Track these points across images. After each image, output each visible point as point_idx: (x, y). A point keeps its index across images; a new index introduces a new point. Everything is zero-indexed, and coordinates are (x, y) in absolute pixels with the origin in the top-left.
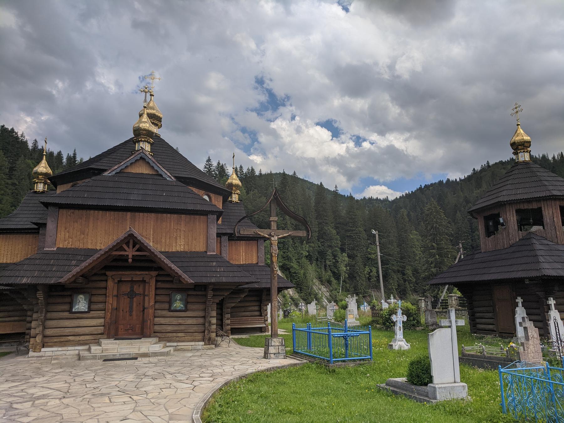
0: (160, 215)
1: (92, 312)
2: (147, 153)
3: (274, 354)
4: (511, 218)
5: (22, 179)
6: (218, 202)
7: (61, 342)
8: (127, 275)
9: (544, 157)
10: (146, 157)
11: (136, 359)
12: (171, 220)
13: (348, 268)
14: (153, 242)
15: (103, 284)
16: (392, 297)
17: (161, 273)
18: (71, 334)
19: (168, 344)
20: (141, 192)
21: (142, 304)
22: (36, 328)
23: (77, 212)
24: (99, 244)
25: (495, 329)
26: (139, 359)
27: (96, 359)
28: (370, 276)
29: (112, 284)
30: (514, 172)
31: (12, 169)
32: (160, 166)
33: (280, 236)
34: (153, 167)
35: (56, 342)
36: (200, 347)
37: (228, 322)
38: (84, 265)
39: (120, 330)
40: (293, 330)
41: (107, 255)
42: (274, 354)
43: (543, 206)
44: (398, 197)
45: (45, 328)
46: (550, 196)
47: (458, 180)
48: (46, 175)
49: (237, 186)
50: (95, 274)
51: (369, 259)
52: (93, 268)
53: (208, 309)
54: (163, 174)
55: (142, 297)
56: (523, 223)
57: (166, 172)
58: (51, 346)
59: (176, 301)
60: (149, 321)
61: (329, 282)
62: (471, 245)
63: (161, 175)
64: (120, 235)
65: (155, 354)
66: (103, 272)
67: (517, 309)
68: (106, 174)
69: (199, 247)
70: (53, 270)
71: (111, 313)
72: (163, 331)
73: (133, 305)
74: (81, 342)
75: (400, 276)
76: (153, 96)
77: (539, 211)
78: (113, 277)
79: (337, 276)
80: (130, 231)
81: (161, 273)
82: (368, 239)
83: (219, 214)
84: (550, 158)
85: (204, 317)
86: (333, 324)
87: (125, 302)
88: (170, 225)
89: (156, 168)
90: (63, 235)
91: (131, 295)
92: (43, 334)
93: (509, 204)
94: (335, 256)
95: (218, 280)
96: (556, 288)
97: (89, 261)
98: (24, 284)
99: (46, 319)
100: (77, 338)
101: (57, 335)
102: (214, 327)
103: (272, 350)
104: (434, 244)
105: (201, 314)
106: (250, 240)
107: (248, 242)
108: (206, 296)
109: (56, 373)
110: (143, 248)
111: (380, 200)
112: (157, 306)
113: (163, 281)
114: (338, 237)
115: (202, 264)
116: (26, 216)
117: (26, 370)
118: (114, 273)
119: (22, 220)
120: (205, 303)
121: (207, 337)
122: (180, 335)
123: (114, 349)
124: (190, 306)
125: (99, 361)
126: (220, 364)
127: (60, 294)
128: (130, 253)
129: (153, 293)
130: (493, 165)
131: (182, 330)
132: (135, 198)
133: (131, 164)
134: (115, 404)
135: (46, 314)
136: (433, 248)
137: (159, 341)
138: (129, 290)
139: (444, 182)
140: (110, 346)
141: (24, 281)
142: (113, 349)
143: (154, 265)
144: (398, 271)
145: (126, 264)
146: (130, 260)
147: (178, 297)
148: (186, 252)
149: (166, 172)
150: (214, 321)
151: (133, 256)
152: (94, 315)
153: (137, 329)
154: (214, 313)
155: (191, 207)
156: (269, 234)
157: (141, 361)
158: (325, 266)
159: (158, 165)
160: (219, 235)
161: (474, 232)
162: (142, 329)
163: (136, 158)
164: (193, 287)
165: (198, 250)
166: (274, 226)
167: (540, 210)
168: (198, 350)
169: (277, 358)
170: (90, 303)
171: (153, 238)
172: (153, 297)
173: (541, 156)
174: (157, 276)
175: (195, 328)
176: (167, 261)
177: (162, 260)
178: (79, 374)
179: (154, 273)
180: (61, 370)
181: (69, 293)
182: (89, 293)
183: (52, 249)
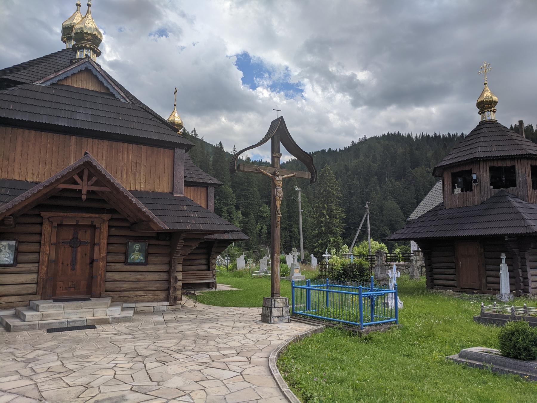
0: (115, 144)
3: (278, 317)
4: (482, 175)
8: (71, 218)
9: (409, 136)
10: (92, 69)
11: (93, 327)
13: (242, 224)
15: (37, 228)
16: (327, 252)
17: (116, 216)
19: (125, 305)
24: (30, 175)
25: (456, 285)
28: (261, 232)
30: (483, 130)
34: (101, 83)
36: (164, 308)
42: (278, 317)
43: (516, 164)
44: (285, 162)
46: (527, 154)
47: (338, 150)
50: (24, 215)
51: (261, 217)
52: (25, 207)
55: (89, 247)
56: (495, 183)
57: (119, 91)
59: (134, 252)
62: (348, 208)
63: (113, 95)
65: (118, 320)
66: (36, 212)
67: (501, 265)
69: (163, 186)
71: (47, 267)
72: (117, 289)
74: (4, 305)
75: (287, 233)
76: (80, 6)
77: (512, 170)
81: (116, 216)
82: (261, 199)
84: (414, 137)
91: (75, 243)
93: (489, 160)
96: (532, 246)
97: (25, 194)
104: (325, 205)
105: (165, 268)
110: (102, 179)
112: (110, 258)
114: (234, 195)
115: (171, 207)
118: (52, 214)
121: (172, 295)
122: (138, 293)
123: (59, 314)
124: (151, 259)
125: (40, 332)
128: (85, 186)
129: (104, 241)
130: (369, 139)
132: (82, 118)
133: (73, 75)
136: (324, 208)
138: (71, 237)
139: (326, 151)
140: (51, 311)
142: (57, 314)
144: (286, 229)
146: (84, 197)
147: (137, 247)
148: (148, 193)
149: (119, 91)
152: (24, 269)
155: (155, 137)
161: (352, 197)
163: (80, 68)
165: (161, 190)
167: (514, 167)
168: (162, 313)
169: (281, 322)
170: (17, 252)
172: (105, 246)
173: (407, 134)
175: (158, 285)
176: (134, 200)
177: (130, 198)
179: (107, 217)
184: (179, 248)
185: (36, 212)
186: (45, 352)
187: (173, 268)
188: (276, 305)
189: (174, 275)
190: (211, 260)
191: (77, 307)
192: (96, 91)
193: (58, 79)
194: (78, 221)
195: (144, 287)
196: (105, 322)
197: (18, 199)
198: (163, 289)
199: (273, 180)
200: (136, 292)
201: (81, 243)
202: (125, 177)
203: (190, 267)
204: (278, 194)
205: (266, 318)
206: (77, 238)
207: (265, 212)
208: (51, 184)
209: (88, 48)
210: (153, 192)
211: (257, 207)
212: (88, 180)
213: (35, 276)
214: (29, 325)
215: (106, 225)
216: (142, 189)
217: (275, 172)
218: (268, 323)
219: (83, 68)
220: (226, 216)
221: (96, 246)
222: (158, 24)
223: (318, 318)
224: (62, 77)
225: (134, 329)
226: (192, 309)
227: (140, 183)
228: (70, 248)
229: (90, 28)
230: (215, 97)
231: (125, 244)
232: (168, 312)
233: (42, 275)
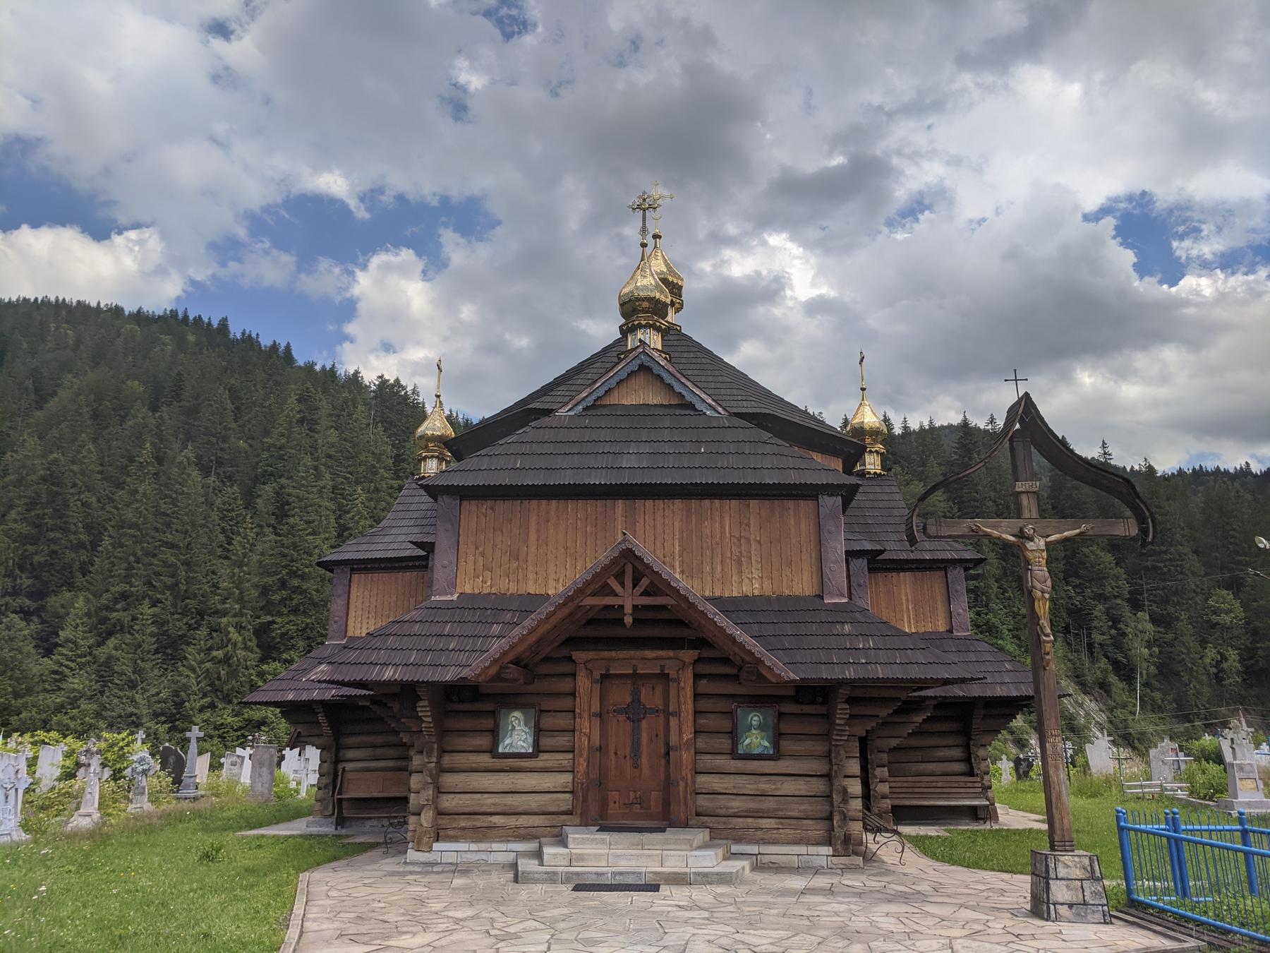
0: (694, 503)
1: (543, 756)
2: (656, 354)
3: (1071, 906)
7: (476, 828)
8: (623, 661)
11: (655, 888)
12: (722, 519)
13: (1156, 649)
14: (682, 572)
15: (565, 685)
17: (707, 653)
18: (498, 809)
19: (735, 848)
20: (647, 448)
22: (419, 790)
23: (500, 505)
24: (552, 583)
26: (664, 890)
27: (555, 882)
28: (1222, 670)
31: (398, 459)
32: (688, 384)
34: (670, 387)
35: (464, 828)
36: (823, 862)
37: (884, 788)
38: (517, 632)
39: (611, 805)
40: (1121, 829)
41: (572, 606)
42: (1071, 906)
45: (439, 791)
50: (546, 659)
51: (1214, 626)
53: (838, 754)
54: (695, 401)
55: (661, 719)
57: (703, 396)
58: (454, 839)
60: (682, 784)
61: (1104, 686)
63: (691, 406)
64: (603, 555)
65: (706, 879)
66: (565, 652)
69: (801, 584)
70: (451, 647)
73: (639, 739)
74: (522, 832)
76: (660, 237)
78: (589, 665)
79: (1126, 672)
80: (624, 541)
81: (707, 653)
82: (1206, 574)
85: (828, 776)
86: (1185, 804)
87: (620, 730)
88: (722, 527)
89: (678, 388)
90: (471, 566)
91: (635, 712)
94: (1115, 621)
98: (388, 683)
99: (443, 771)
100: (512, 821)
101: (467, 810)
102: (857, 804)
103: (1059, 891)
106: (925, 569)
107: (919, 574)
108: (828, 717)
109: (457, 921)
110: (658, 586)
111: (1226, 472)
112: (702, 743)
113: (712, 677)
114: (1121, 571)
115: (814, 628)
116: (405, 530)
117: (391, 904)
118: (590, 655)
119: (395, 541)
120: (827, 736)
121: (839, 833)
124: (787, 745)
125: (563, 888)
126: (901, 928)
127: (466, 707)
128: (628, 599)
129: (688, 706)
131: (769, 810)
132: (633, 464)
135: (439, 757)
138: (628, 700)
141: (388, 674)
142: (595, 855)
143: (686, 633)
145: (617, 632)
146: (628, 620)
147: (755, 719)
148: (768, 599)
149: (703, 396)
150: (855, 787)
151: (635, 607)
152: (550, 764)
153: (652, 803)
154: (854, 767)
156: (1016, 531)
157: (672, 896)
158: (1090, 646)
159: (683, 380)
160: (851, 555)
162: (667, 803)
163: (629, 369)
164: (791, 692)
166: (1029, 507)
168: (817, 871)
169: (1080, 919)
170: (538, 732)
172: (691, 717)
174: (695, 662)
175: (805, 807)
176: (721, 620)
178: (512, 930)
179: (689, 655)
180: (469, 912)
181: (488, 706)
182: (533, 706)
183: (448, 598)
184: (842, 722)
185: (565, 652)
186: (543, 926)
187: (835, 768)
188: (1062, 872)
189: (836, 783)
190: (973, 749)
191: (634, 845)
192: (661, 405)
193: (593, 397)
196: (679, 879)
199: (1022, 548)
200: (760, 821)
201: (646, 712)
202: (719, 569)
203: (922, 767)
204: (1037, 584)
205: (1040, 907)
206: (639, 701)
207: (1228, 612)
208: (569, 599)
209: (645, 326)
210: (780, 597)
211: (1198, 599)
212: (634, 586)
213: (568, 777)
214: (547, 873)
215: (689, 673)
216: (757, 593)
217: (1021, 530)
218: (1042, 918)
219: (634, 366)
220: (1105, 629)
221: (671, 718)
222: (901, 193)
223: (1195, 920)
224: (601, 393)
225: (727, 900)
226: (892, 868)
229: (645, 288)
230: (1075, 320)
231: (730, 713)
232: (830, 870)
233: (580, 776)
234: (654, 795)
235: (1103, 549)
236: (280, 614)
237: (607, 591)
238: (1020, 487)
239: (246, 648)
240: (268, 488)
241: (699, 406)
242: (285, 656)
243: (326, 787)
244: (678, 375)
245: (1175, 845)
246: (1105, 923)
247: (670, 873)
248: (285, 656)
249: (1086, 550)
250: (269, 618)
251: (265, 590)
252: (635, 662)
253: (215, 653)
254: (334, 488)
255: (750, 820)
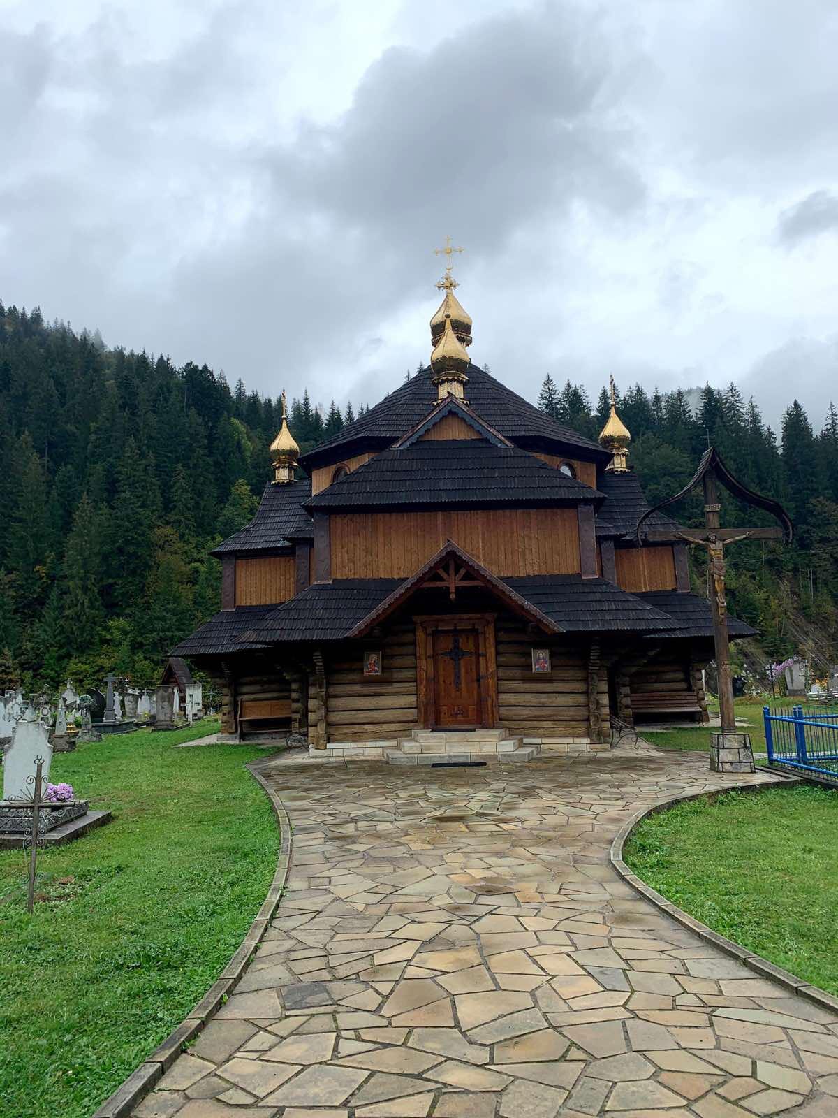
3: (731, 763)
5: (229, 454)
6: (588, 476)
15: (409, 637)
18: (369, 720)
19: (526, 741)
21: (474, 670)
23: (357, 518)
24: (396, 571)
29: (424, 637)
33: (728, 541)
34: (471, 427)
35: (347, 734)
37: (627, 701)
42: (731, 763)
45: (328, 711)
48: (291, 454)
49: (621, 440)
53: (593, 678)
55: (474, 658)
63: (487, 440)
64: (435, 551)
68: (395, 447)
69: (566, 564)
72: (515, 717)
73: (459, 671)
74: (385, 734)
83: (598, 504)
85: (586, 693)
90: (339, 559)
91: (456, 654)
92: (327, 721)
95: (607, 627)
99: (329, 696)
100: (378, 728)
102: (606, 711)
103: (725, 756)
110: (472, 573)
118: (424, 618)
122: (545, 724)
128: (452, 583)
132: (447, 488)
133: (435, 425)
134: (478, 834)
135: (327, 688)
137: (510, 735)
138: (451, 646)
146: (453, 596)
150: (605, 700)
151: (457, 588)
152: (401, 690)
154: (604, 687)
156: (705, 537)
160: (600, 540)
162: (480, 712)
165: (563, 571)
166: (714, 521)
171: (484, 556)
175: (572, 713)
176: (514, 595)
187: (591, 687)
190: (692, 673)
193: (416, 436)
194: (455, 624)
195: (553, 715)
197: (383, 606)
198: (582, 718)
203: (656, 686)
213: (413, 698)
216: (536, 574)
221: (481, 658)
227: (531, 564)
228: (451, 661)
234: (471, 708)
235: (828, 499)
236: (118, 576)
237: (438, 578)
238: (708, 508)
239: (92, 607)
240: (99, 467)
241: (493, 441)
242: (127, 611)
243: (229, 713)
244: (477, 418)
245: (799, 728)
246: (752, 772)
247: (486, 755)
248: (127, 611)
249: (813, 501)
250: (111, 581)
251: (105, 557)
252: (455, 622)
253: (67, 612)
254: (157, 466)
255: (535, 722)
